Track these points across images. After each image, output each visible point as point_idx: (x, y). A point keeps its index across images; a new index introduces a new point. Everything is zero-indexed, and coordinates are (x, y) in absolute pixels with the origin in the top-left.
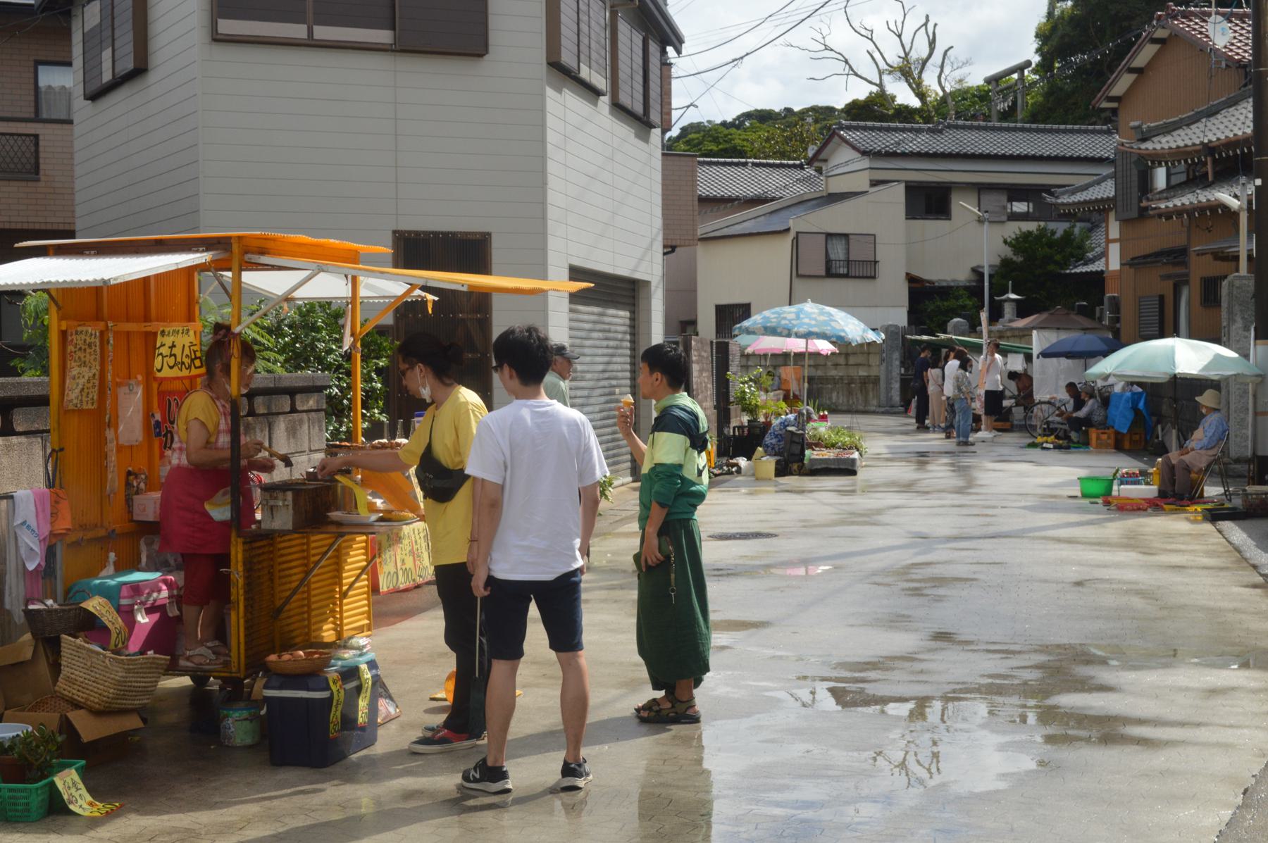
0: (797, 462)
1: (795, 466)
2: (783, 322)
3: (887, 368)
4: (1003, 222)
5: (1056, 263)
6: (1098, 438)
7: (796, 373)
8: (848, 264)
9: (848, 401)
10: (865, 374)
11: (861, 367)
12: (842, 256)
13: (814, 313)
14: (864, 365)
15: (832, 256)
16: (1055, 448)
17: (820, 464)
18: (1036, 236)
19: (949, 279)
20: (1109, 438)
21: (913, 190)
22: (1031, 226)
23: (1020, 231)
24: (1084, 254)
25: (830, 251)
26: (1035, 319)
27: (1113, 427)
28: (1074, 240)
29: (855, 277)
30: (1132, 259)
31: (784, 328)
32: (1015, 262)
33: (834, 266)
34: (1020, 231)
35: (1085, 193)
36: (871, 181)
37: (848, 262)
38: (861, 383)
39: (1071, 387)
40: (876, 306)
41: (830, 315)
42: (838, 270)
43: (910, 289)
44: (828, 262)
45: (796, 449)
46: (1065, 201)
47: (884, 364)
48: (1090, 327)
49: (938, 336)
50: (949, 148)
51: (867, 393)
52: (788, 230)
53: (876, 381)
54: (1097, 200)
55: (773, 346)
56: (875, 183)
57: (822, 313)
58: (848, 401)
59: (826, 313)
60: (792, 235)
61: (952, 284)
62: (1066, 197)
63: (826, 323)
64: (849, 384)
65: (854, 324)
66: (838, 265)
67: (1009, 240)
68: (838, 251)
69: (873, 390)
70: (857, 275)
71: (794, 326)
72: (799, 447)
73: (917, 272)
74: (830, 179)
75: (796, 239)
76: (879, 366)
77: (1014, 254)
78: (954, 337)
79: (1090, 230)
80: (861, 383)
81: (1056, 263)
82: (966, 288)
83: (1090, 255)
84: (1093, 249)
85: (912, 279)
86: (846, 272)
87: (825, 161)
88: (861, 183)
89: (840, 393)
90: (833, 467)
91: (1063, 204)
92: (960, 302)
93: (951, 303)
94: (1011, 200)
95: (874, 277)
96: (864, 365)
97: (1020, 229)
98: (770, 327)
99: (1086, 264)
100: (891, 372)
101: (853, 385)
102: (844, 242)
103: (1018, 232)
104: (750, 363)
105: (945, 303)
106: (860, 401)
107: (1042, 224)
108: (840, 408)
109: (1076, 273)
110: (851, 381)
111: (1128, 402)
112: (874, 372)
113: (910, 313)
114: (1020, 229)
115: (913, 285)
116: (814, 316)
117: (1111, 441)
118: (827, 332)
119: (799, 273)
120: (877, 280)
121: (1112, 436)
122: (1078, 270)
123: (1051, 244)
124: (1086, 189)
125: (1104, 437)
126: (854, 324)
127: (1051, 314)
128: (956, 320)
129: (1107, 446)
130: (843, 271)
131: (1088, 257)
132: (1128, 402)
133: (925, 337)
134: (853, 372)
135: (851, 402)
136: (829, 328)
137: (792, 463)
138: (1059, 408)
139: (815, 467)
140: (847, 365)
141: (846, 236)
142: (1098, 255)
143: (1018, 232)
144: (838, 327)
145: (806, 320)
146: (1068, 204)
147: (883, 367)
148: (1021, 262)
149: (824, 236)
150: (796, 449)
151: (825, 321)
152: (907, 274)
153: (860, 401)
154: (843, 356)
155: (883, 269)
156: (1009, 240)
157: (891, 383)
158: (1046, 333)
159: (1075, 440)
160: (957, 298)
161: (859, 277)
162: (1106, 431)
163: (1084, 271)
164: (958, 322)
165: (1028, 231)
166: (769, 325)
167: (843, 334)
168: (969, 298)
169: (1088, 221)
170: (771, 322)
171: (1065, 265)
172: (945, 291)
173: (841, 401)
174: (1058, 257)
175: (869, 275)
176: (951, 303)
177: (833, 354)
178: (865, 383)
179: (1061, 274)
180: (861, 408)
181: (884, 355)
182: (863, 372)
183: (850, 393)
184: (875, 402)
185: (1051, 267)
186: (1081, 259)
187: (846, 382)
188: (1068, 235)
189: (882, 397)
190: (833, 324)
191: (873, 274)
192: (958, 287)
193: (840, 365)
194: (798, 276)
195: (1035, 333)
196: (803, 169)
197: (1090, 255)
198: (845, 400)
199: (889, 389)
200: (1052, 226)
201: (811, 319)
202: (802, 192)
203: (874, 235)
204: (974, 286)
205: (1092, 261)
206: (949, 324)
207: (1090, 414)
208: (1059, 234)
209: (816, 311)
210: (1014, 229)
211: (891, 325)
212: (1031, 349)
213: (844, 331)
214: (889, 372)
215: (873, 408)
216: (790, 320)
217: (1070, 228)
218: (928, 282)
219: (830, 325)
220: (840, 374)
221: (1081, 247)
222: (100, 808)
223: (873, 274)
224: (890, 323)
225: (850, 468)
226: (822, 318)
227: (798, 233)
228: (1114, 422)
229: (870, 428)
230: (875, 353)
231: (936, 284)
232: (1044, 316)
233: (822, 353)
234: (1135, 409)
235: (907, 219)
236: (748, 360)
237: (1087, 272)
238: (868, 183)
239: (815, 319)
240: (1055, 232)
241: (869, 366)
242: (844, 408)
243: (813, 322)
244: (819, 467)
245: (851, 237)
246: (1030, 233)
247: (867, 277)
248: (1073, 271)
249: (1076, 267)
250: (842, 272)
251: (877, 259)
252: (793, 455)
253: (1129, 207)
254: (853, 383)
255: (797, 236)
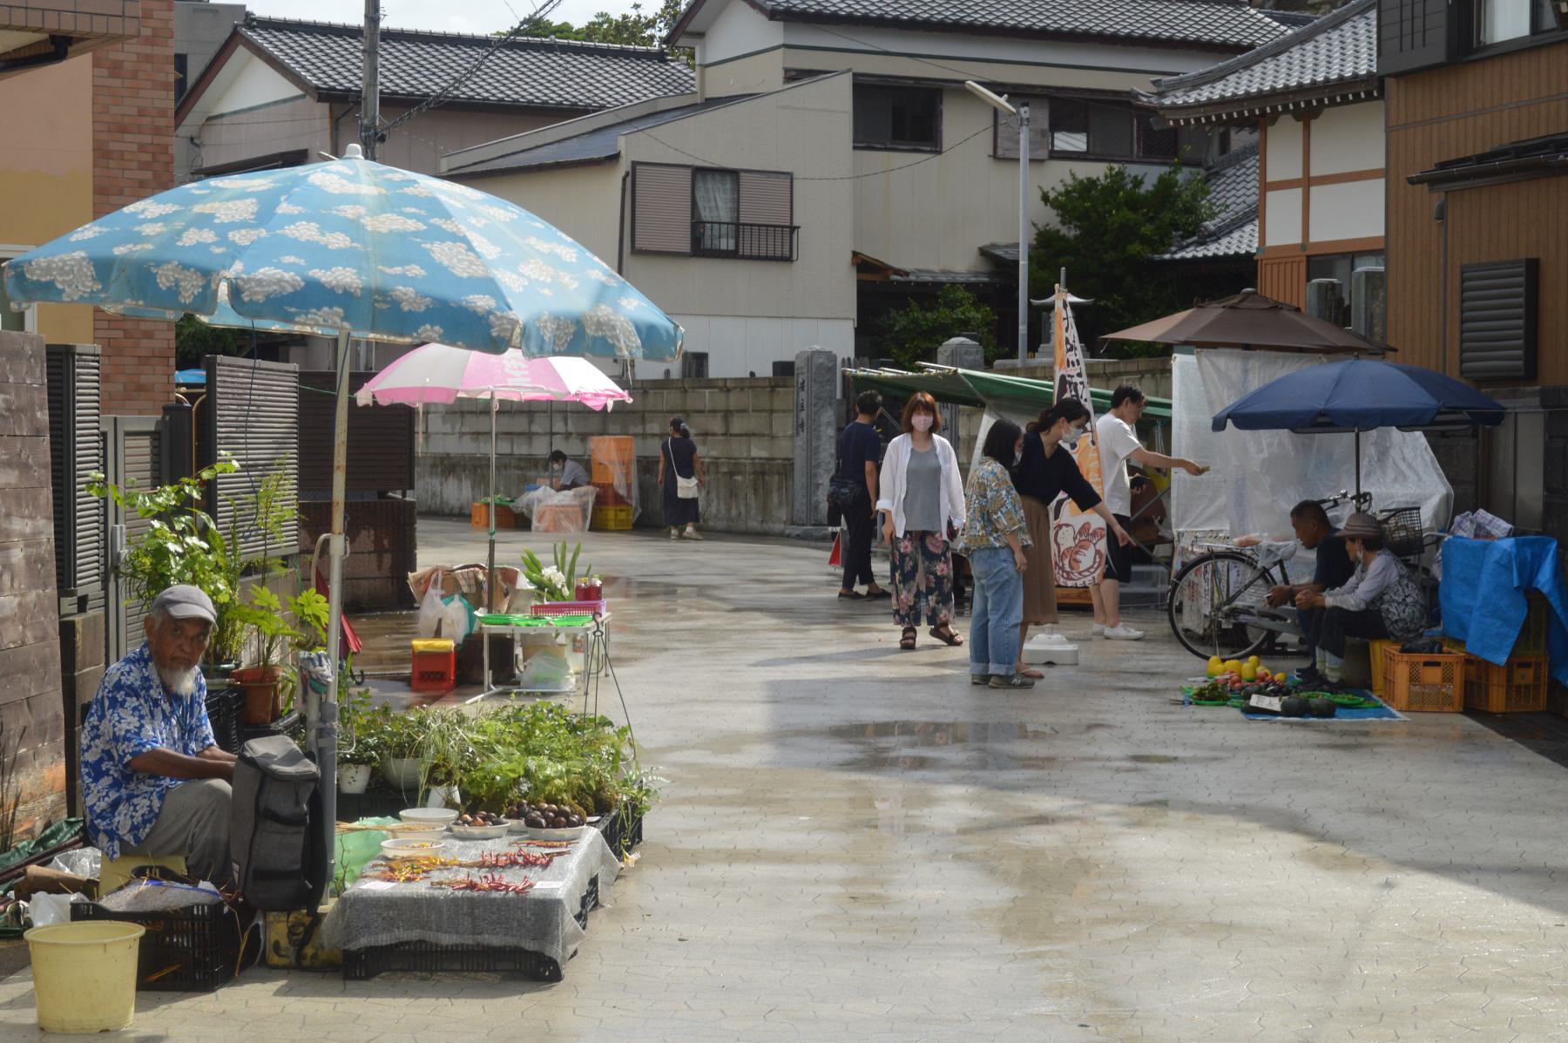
0: (288, 907)
1: (276, 929)
2: (191, 237)
3: (809, 442)
4: (1042, 161)
5: (1145, 240)
6: (1414, 679)
7: (620, 450)
8: (737, 231)
9: (729, 510)
10: (764, 454)
11: (754, 440)
12: (725, 215)
13: (354, 199)
14: (763, 435)
15: (706, 215)
16: (1287, 711)
17: (390, 925)
18: (1103, 186)
19: (936, 269)
20: (1447, 679)
21: (867, 91)
22: (1097, 171)
23: (1074, 178)
24: (1197, 224)
25: (700, 204)
26: (1184, 321)
27: (1460, 643)
28: (1179, 195)
29: (751, 258)
30: (1442, 165)
31: (185, 267)
32: (1063, 238)
33: (708, 232)
34: (1074, 178)
35: (1219, 86)
36: (786, 70)
37: (737, 225)
38: (754, 473)
39: (1310, 517)
40: (792, 317)
41: (434, 207)
42: (716, 242)
43: (860, 284)
44: (697, 225)
45: (284, 848)
46: (1180, 102)
47: (803, 435)
48: (1340, 344)
49: (921, 369)
50: (939, 13)
51: (767, 494)
52: (615, 158)
53: (786, 469)
54: (1248, 97)
55: (428, 382)
56: (794, 76)
57: (392, 202)
58: (729, 510)
59: (416, 201)
60: (624, 166)
61: (943, 278)
62: (1179, 93)
63: (404, 247)
64: (731, 474)
65: (553, 260)
66: (716, 233)
67: (1052, 195)
68: (716, 204)
69: (780, 489)
70: (763, 253)
71: (236, 252)
72: (298, 840)
73: (873, 252)
74: (709, 70)
75: (632, 179)
76: (792, 436)
77: (1063, 223)
78: (960, 371)
79: (1207, 180)
80: (754, 473)
81: (1145, 240)
82: (969, 286)
83: (1210, 225)
84: (1213, 216)
85: (864, 266)
86: (732, 246)
87: (701, 35)
88: (769, 72)
89: (713, 495)
90: (447, 939)
91: (1174, 108)
92: (958, 313)
93: (943, 315)
94: (1056, 125)
95: (788, 259)
96: (763, 435)
97: (1073, 175)
98: (124, 263)
99: (1202, 243)
100: (816, 451)
101: (739, 478)
102: (728, 186)
103: (1069, 181)
104: (535, 428)
105: (929, 315)
106: (753, 512)
107: (1116, 166)
108: (711, 523)
109: (1183, 260)
110: (735, 468)
111: (1508, 568)
112: (782, 450)
113: (860, 332)
114: (1073, 175)
115: (869, 277)
116: (349, 211)
117: (1454, 690)
118: (401, 290)
119: (638, 245)
120: (795, 264)
121: (1458, 672)
122: (1188, 254)
123: (1134, 203)
124: (1222, 78)
125: (1433, 675)
126: (553, 260)
127: (1231, 307)
128: (955, 340)
129: (1440, 705)
130: (726, 244)
131: (1206, 228)
132: (1508, 568)
133: (888, 373)
134: (739, 450)
135: (734, 512)
136: (416, 271)
137: (267, 908)
138: (1265, 574)
139: (364, 941)
140: (725, 434)
141: (734, 174)
142: (1227, 226)
143: (1069, 181)
144: (462, 270)
145: (306, 231)
146: (1187, 107)
147: (800, 441)
148: (1076, 237)
149: (689, 171)
150: (284, 848)
151: (403, 235)
152: (855, 254)
153: (753, 512)
154: (719, 415)
155: (806, 242)
156: (1052, 195)
157: (815, 475)
158: (1227, 363)
159: (1333, 677)
160: (952, 305)
161: (767, 258)
162: (1437, 657)
163: (1200, 255)
164: (961, 344)
165: (1088, 179)
166: (119, 251)
167: (482, 302)
168: (976, 305)
169: (1197, 164)
170: (138, 238)
171: (1162, 243)
172: (929, 293)
173: (713, 510)
174: (1147, 229)
175: (778, 253)
176: (943, 315)
177: (620, 405)
178: (763, 473)
179: (1152, 262)
180: (754, 524)
181: (803, 415)
182: (758, 451)
183: (733, 493)
184: (783, 514)
185: (1135, 248)
186: (1193, 234)
187: (725, 469)
188: (1165, 185)
189: (797, 505)
190: (441, 252)
191: (787, 253)
192: (953, 284)
193: (714, 435)
194: (635, 252)
195: (1181, 363)
196: (665, 61)
197: (1210, 225)
198: (723, 508)
199: (811, 487)
200: (1133, 170)
201: (329, 224)
202: (652, 96)
203: (790, 176)
204: (985, 284)
205: (1216, 236)
206: (940, 349)
207: (1378, 599)
208: (1148, 186)
209: (367, 189)
210: (1059, 176)
211: (818, 352)
212: (1169, 406)
213: (490, 286)
214: (812, 451)
215: (778, 527)
216: (222, 230)
217: (1170, 173)
218: (897, 272)
219: (426, 261)
220: (714, 453)
221: (1190, 210)
222: (695, 535)
223: (787, 253)
224: (817, 347)
225: (529, 945)
226: (391, 222)
227: (635, 164)
228: (1464, 628)
229: (756, 593)
230: (784, 411)
231: (912, 278)
232: (1213, 312)
233: (590, 404)
234: (1529, 592)
235: (855, 148)
236: (531, 422)
237: (1205, 257)
238: (781, 74)
239: (353, 227)
240: (1141, 182)
241: (773, 437)
242: (721, 525)
243: (339, 241)
244: (384, 939)
245: (742, 174)
246: (1092, 183)
247: (774, 259)
248: (1178, 256)
249: (1182, 248)
250: (723, 247)
251: (795, 224)
252: (262, 875)
253: (1418, 38)
254: (739, 473)
255: (634, 169)
